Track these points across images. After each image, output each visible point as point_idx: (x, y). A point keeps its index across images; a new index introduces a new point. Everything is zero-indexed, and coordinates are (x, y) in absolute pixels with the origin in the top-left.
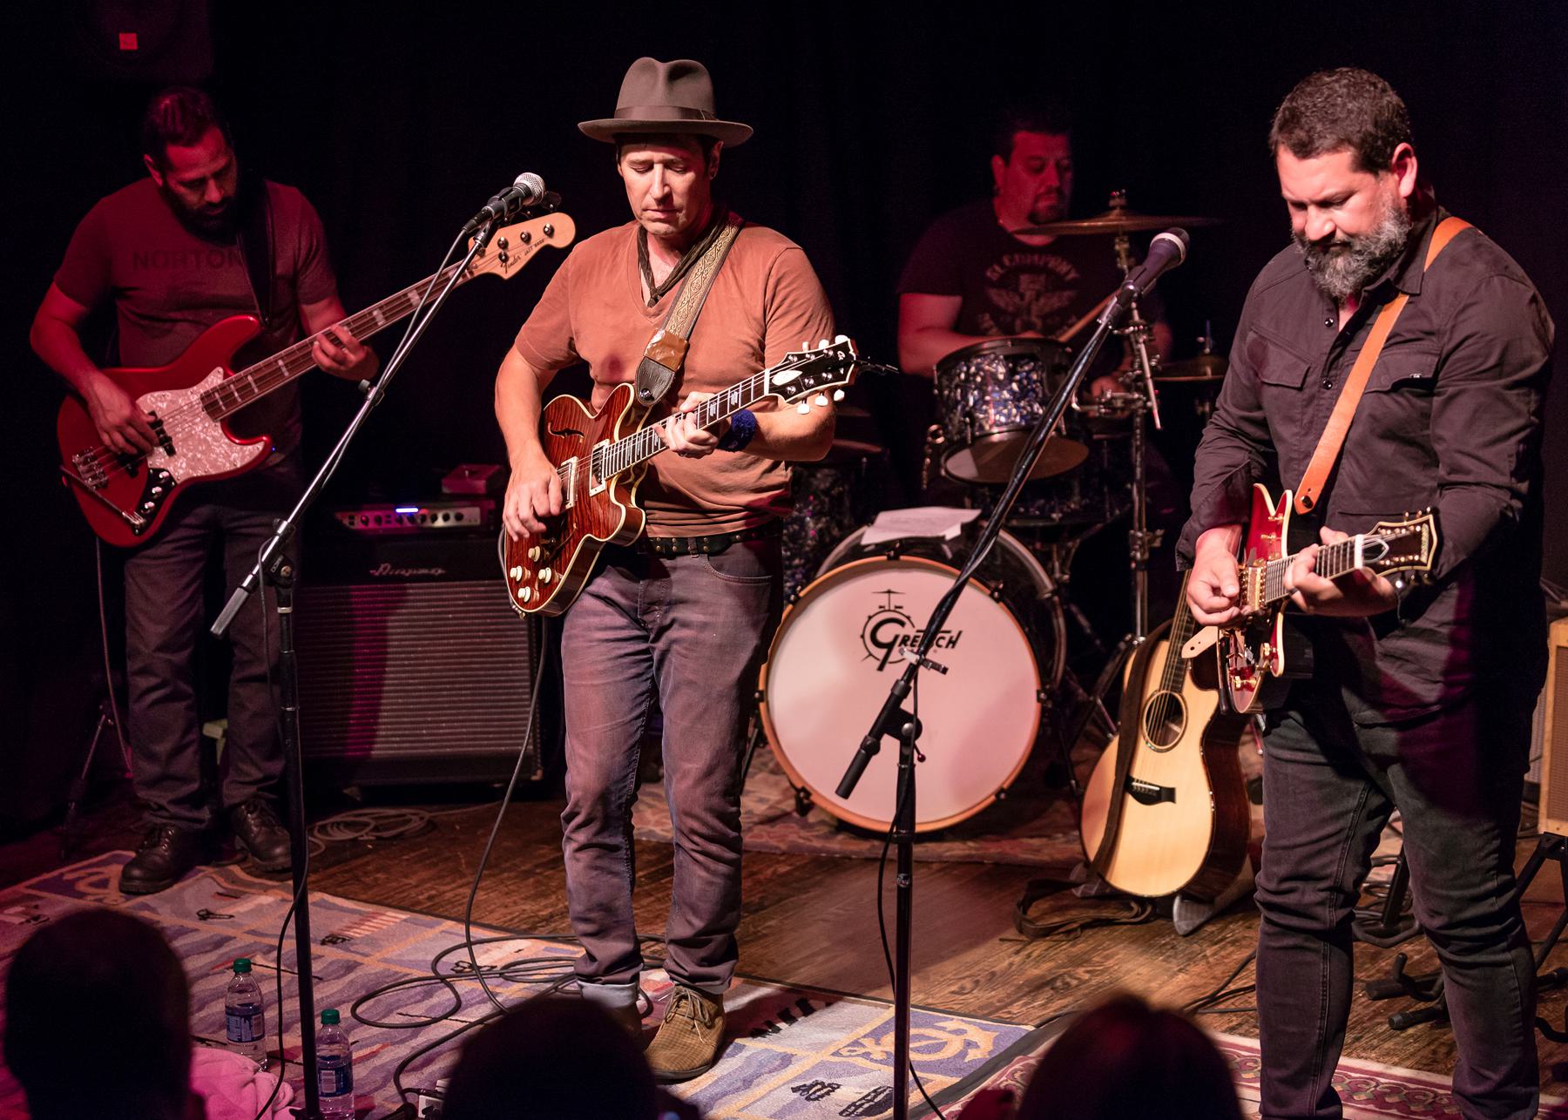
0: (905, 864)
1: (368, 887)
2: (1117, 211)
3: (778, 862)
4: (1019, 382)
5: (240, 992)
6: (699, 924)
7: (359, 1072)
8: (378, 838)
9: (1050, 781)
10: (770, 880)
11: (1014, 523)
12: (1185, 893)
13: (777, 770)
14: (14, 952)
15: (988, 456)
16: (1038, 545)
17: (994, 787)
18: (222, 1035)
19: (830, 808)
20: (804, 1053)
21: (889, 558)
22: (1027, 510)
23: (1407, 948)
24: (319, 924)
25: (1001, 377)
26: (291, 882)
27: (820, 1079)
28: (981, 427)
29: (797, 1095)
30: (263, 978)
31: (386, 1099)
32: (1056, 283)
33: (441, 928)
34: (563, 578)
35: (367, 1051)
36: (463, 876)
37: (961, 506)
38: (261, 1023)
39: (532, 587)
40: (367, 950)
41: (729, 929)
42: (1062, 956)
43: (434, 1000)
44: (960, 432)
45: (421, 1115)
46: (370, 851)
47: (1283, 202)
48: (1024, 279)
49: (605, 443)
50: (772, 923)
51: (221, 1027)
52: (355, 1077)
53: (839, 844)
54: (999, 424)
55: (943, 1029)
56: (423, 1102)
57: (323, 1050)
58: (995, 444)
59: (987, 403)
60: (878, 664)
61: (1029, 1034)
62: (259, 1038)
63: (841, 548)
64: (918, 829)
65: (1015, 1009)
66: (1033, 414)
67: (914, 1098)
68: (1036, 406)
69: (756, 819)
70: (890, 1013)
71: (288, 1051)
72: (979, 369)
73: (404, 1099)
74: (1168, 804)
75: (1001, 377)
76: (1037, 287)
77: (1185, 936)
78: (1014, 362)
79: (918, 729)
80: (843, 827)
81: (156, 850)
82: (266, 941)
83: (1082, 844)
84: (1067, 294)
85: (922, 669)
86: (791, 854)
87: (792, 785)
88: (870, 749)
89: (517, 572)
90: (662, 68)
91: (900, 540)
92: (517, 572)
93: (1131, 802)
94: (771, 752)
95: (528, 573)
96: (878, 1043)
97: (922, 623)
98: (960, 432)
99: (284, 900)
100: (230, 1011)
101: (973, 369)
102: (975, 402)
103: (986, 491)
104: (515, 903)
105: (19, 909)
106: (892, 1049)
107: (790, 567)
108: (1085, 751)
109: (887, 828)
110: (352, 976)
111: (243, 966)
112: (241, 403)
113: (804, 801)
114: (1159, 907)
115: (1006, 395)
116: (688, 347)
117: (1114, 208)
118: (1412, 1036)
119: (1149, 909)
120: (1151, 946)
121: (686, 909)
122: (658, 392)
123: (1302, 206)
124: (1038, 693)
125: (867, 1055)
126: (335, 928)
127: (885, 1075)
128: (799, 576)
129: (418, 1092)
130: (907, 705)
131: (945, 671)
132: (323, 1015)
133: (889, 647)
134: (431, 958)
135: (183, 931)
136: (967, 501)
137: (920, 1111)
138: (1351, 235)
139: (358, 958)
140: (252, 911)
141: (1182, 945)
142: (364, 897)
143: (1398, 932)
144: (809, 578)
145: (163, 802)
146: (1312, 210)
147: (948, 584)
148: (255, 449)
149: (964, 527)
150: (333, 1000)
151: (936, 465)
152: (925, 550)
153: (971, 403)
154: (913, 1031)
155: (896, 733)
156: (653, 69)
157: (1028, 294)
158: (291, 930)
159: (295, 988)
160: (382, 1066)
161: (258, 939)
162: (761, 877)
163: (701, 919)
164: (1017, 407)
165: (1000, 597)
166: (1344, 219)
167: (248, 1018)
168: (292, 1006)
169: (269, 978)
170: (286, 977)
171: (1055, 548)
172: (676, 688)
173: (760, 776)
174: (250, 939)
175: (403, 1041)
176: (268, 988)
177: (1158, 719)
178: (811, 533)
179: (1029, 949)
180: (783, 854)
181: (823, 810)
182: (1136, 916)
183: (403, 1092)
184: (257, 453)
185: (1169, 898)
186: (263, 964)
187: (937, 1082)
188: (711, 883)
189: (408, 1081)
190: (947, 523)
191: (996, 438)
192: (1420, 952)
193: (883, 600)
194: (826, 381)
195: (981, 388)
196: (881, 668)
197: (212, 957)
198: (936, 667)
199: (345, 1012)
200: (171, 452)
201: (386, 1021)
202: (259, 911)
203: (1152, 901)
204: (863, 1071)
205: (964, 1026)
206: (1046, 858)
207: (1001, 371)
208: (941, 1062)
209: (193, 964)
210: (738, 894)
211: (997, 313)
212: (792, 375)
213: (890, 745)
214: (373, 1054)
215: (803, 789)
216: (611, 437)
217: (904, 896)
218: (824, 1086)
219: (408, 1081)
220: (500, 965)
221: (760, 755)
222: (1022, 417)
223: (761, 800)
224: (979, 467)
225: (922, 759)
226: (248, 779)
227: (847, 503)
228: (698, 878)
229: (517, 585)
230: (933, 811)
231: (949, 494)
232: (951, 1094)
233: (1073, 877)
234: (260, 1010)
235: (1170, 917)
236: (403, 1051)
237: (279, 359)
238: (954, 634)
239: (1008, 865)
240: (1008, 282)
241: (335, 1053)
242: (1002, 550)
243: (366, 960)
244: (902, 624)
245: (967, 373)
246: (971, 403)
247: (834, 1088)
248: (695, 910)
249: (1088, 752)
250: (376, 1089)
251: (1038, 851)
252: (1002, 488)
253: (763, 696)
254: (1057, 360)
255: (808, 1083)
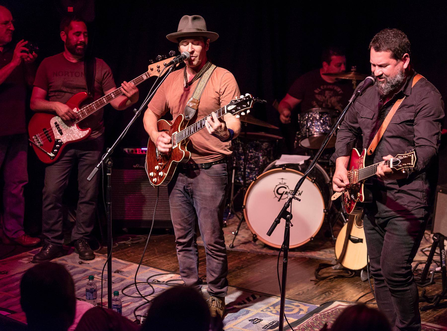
0: (286, 256)
1: (129, 257)
2: (353, 73)
3: (248, 255)
4: (323, 120)
5: (90, 285)
6: (216, 276)
7: (124, 310)
8: (133, 243)
9: (325, 237)
10: (245, 260)
11: (319, 161)
12: (365, 269)
13: (248, 229)
14: (25, 271)
15: (313, 140)
16: (326, 167)
17: (310, 237)
18: (85, 298)
19: (262, 240)
20: (253, 310)
21: (283, 169)
22: (323, 157)
23: (428, 288)
24: (115, 267)
25: (318, 118)
26: (107, 255)
27: (257, 317)
28: (311, 133)
29: (250, 322)
30: (97, 282)
31: (131, 318)
32: (336, 94)
33: (149, 270)
34: (166, 174)
35: (127, 304)
36: (156, 255)
37: (304, 155)
38: (96, 295)
39: (157, 178)
40: (128, 275)
41: (225, 276)
42: (328, 286)
43: (146, 290)
44: (305, 134)
45: (141, 323)
46: (130, 247)
47: (370, 64)
48: (327, 92)
49: (176, 133)
50: (245, 272)
51: (84, 295)
52: (123, 311)
53: (264, 251)
54: (317, 132)
55: (293, 305)
56: (142, 319)
57: (114, 303)
58: (315, 137)
59: (313, 125)
60: (278, 199)
61: (318, 307)
62: (95, 299)
63: (270, 166)
64: (290, 247)
65: (314, 300)
66: (326, 130)
67: (285, 324)
68: (327, 127)
69: (241, 242)
70: (279, 299)
71: (104, 303)
72: (311, 116)
73: (136, 318)
74: (360, 244)
75: (318, 118)
76: (330, 94)
77: (364, 281)
78: (321, 114)
79: (291, 217)
80: (266, 246)
81: (45, 251)
82: (98, 271)
83: (335, 254)
84: (339, 97)
85: (293, 199)
86: (251, 252)
87: (252, 233)
88: (277, 222)
89: (152, 174)
90: (190, 17)
91: (287, 164)
92: (152, 174)
93: (350, 242)
94: (246, 224)
95: (155, 174)
96: (274, 308)
97: (293, 189)
98: (305, 134)
99: (104, 260)
100: (87, 290)
101: (310, 116)
102: (310, 125)
103: (312, 151)
104: (171, 263)
105: (27, 259)
106: (279, 310)
107: (254, 170)
108: (337, 227)
109: (280, 247)
110: (123, 282)
111: (91, 278)
112: (82, 118)
113: (255, 238)
114: (357, 273)
115: (319, 123)
116: (199, 102)
117: (352, 71)
118: (428, 313)
119: (354, 273)
120: (354, 284)
121: (211, 272)
122: (191, 116)
123: (375, 65)
124: (324, 210)
125: (271, 311)
126: (119, 268)
127: (277, 318)
128: (257, 173)
129: (141, 316)
130: (288, 210)
131: (300, 200)
132: (114, 293)
133: (282, 194)
134: (147, 278)
135: (74, 267)
136: (306, 154)
137: (287, 328)
138: (387, 76)
139: (125, 277)
140: (95, 262)
141: (363, 284)
142: (127, 260)
143: (425, 283)
144: (259, 174)
145: (50, 237)
146: (377, 67)
147: (299, 177)
148: (86, 132)
149: (305, 161)
150: (117, 289)
151: (298, 143)
152: (293, 167)
153: (309, 125)
154: (285, 305)
155: (285, 218)
156: (187, 18)
157: (328, 97)
158: (106, 268)
159: (106, 285)
160: (131, 308)
161: (95, 270)
162: (242, 259)
163: (217, 274)
164: (322, 127)
165: (315, 182)
166: (385, 70)
167: (92, 293)
168: (106, 290)
169: (99, 282)
170: (104, 282)
171: (331, 168)
172: (201, 209)
173: (243, 230)
174: (93, 270)
175: (137, 302)
176: (99, 285)
177: (359, 219)
178: (261, 161)
179: (319, 283)
180: (249, 253)
181: (260, 241)
182: (350, 275)
183: (136, 316)
184: (87, 133)
185: (360, 270)
186: (97, 278)
187: (291, 320)
188: (219, 263)
189: (138, 313)
190: (300, 160)
191: (315, 136)
192: (431, 289)
193: (281, 181)
194: (244, 107)
195: (312, 121)
196: (279, 201)
197: (83, 275)
198: (297, 199)
199: (120, 293)
200: (61, 134)
201: (132, 295)
202: (97, 262)
203: (355, 271)
204: (270, 316)
205: (299, 304)
206: (324, 258)
207: (318, 117)
208: (292, 314)
209: (75, 277)
210: (227, 267)
211: (318, 101)
212: (234, 106)
213: (283, 221)
214: (128, 305)
215: (255, 235)
216: (178, 131)
217: (285, 265)
218: (258, 320)
219: (138, 313)
220: (166, 281)
221: (243, 224)
222: (323, 130)
223: (243, 237)
224: (310, 143)
225: (292, 226)
226: (81, 233)
227: (272, 153)
228: (214, 264)
229: (152, 178)
230: (293, 243)
231: (301, 151)
232: (296, 323)
233: (332, 263)
234: (96, 291)
235: (360, 276)
236: (137, 305)
237: (93, 105)
238: (301, 192)
239: (313, 259)
240: (322, 93)
241: (117, 304)
242: (316, 168)
243: (127, 278)
244: (286, 188)
245: (308, 117)
246: (309, 125)
247: (261, 320)
248: (214, 271)
249: (338, 228)
250: (129, 315)
251: (322, 255)
252: (317, 150)
253: (245, 207)
254: (334, 114)
255: (253, 318)
